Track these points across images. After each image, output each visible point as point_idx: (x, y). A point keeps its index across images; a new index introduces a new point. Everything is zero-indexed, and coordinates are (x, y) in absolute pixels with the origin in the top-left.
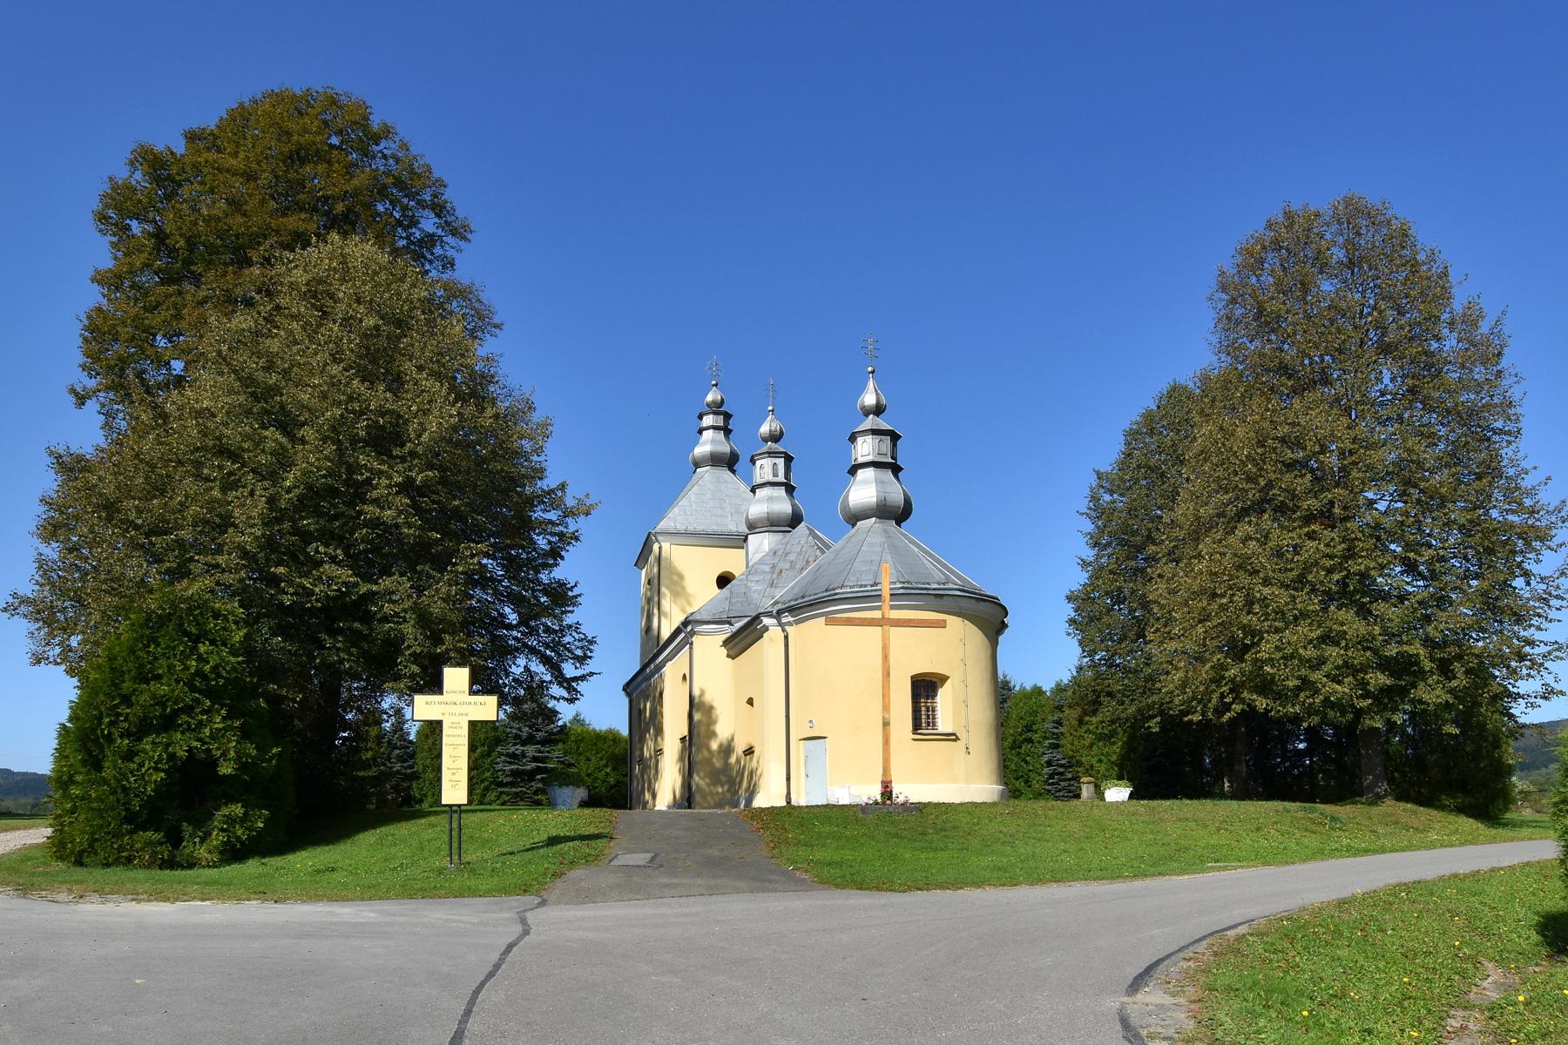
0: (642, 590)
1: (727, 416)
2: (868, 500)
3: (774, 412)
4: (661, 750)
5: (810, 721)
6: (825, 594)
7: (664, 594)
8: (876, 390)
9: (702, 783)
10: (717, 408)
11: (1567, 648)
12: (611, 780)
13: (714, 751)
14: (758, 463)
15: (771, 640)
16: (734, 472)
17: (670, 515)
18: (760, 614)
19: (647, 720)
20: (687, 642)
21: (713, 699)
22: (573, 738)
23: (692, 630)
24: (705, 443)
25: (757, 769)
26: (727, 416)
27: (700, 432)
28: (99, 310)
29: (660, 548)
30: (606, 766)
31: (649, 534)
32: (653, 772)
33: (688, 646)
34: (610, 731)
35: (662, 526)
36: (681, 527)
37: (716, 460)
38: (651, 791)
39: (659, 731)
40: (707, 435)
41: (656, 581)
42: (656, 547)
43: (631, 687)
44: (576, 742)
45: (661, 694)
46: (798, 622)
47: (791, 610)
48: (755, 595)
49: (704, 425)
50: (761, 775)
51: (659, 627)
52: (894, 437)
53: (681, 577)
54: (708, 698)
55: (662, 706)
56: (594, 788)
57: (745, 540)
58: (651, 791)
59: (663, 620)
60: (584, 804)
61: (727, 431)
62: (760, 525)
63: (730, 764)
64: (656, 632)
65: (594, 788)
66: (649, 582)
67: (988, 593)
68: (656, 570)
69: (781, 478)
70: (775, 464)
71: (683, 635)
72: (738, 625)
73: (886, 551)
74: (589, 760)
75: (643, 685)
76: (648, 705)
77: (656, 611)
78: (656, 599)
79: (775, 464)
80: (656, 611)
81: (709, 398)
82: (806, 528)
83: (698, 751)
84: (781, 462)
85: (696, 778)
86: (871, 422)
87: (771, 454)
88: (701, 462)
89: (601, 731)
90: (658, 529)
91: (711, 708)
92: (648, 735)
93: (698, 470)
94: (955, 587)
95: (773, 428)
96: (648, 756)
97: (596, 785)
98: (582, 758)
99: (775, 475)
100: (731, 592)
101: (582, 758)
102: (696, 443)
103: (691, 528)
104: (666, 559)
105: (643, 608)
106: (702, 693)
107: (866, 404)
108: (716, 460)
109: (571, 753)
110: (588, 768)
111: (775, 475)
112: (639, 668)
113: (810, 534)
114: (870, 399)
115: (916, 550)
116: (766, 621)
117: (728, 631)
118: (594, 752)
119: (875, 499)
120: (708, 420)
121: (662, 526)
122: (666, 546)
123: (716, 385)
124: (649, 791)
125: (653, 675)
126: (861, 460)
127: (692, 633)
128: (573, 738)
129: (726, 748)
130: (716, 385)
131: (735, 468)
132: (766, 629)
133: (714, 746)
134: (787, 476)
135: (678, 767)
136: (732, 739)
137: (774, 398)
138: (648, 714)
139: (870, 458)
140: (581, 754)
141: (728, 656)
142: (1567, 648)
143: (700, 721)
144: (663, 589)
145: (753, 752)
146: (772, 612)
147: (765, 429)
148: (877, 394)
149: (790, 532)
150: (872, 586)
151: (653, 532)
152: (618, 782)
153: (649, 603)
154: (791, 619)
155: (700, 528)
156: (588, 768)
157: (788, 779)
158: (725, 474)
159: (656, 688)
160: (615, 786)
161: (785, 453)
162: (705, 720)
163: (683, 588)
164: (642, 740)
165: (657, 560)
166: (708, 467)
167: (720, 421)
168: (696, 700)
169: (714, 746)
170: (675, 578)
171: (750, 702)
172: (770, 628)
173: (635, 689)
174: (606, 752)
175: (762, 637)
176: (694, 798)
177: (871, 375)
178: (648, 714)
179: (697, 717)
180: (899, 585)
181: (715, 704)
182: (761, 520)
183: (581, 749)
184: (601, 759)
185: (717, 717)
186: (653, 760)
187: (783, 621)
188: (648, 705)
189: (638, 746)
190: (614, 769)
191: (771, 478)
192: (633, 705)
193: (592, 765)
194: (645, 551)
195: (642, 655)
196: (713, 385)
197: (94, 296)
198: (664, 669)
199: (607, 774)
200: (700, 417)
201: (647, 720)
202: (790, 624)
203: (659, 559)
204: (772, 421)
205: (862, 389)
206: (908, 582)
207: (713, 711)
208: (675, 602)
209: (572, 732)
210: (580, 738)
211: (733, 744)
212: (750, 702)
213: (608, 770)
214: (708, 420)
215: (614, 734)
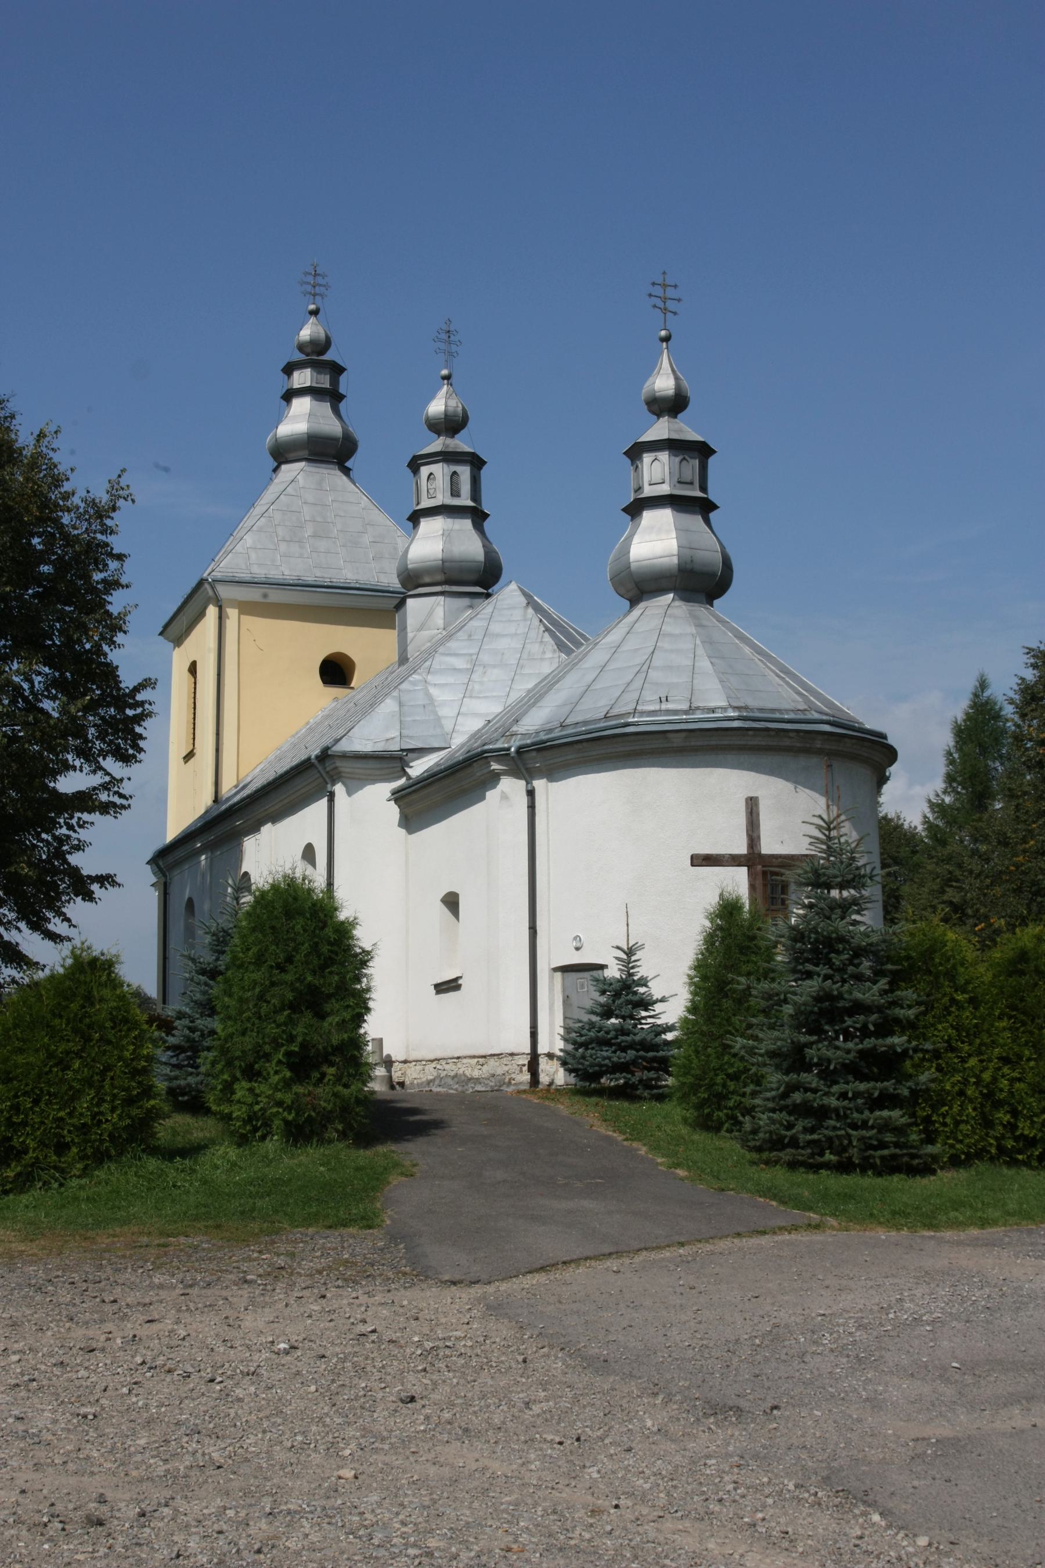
1: (336, 370)
3: (453, 380)
5: (575, 938)
6: (602, 725)
8: (673, 371)
14: (425, 471)
16: (346, 471)
24: (296, 419)
28: (126, 759)
33: (324, 801)
40: (302, 405)
43: (170, 859)
49: (296, 386)
52: (702, 451)
57: (401, 604)
62: (427, 580)
67: (868, 726)
69: (465, 500)
70: (455, 473)
73: (700, 651)
79: (455, 473)
81: (306, 334)
82: (519, 593)
84: (465, 472)
86: (661, 429)
87: (448, 457)
93: (284, 467)
94: (825, 718)
100: (401, 705)
111: (455, 493)
113: (528, 603)
114: (664, 383)
115: (747, 650)
119: (675, 560)
121: (227, 565)
123: (315, 313)
126: (648, 491)
131: (348, 464)
134: (476, 494)
139: (665, 489)
146: (509, 749)
147: (437, 407)
148: (677, 378)
150: (686, 712)
158: (333, 476)
166: (303, 464)
167: (325, 381)
171: (452, 902)
177: (664, 344)
180: (732, 714)
182: (429, 570)
197: (373, 996)
204: (447, 398)
205: (650, 368)
206: (746, 708)
212: (452, 902)
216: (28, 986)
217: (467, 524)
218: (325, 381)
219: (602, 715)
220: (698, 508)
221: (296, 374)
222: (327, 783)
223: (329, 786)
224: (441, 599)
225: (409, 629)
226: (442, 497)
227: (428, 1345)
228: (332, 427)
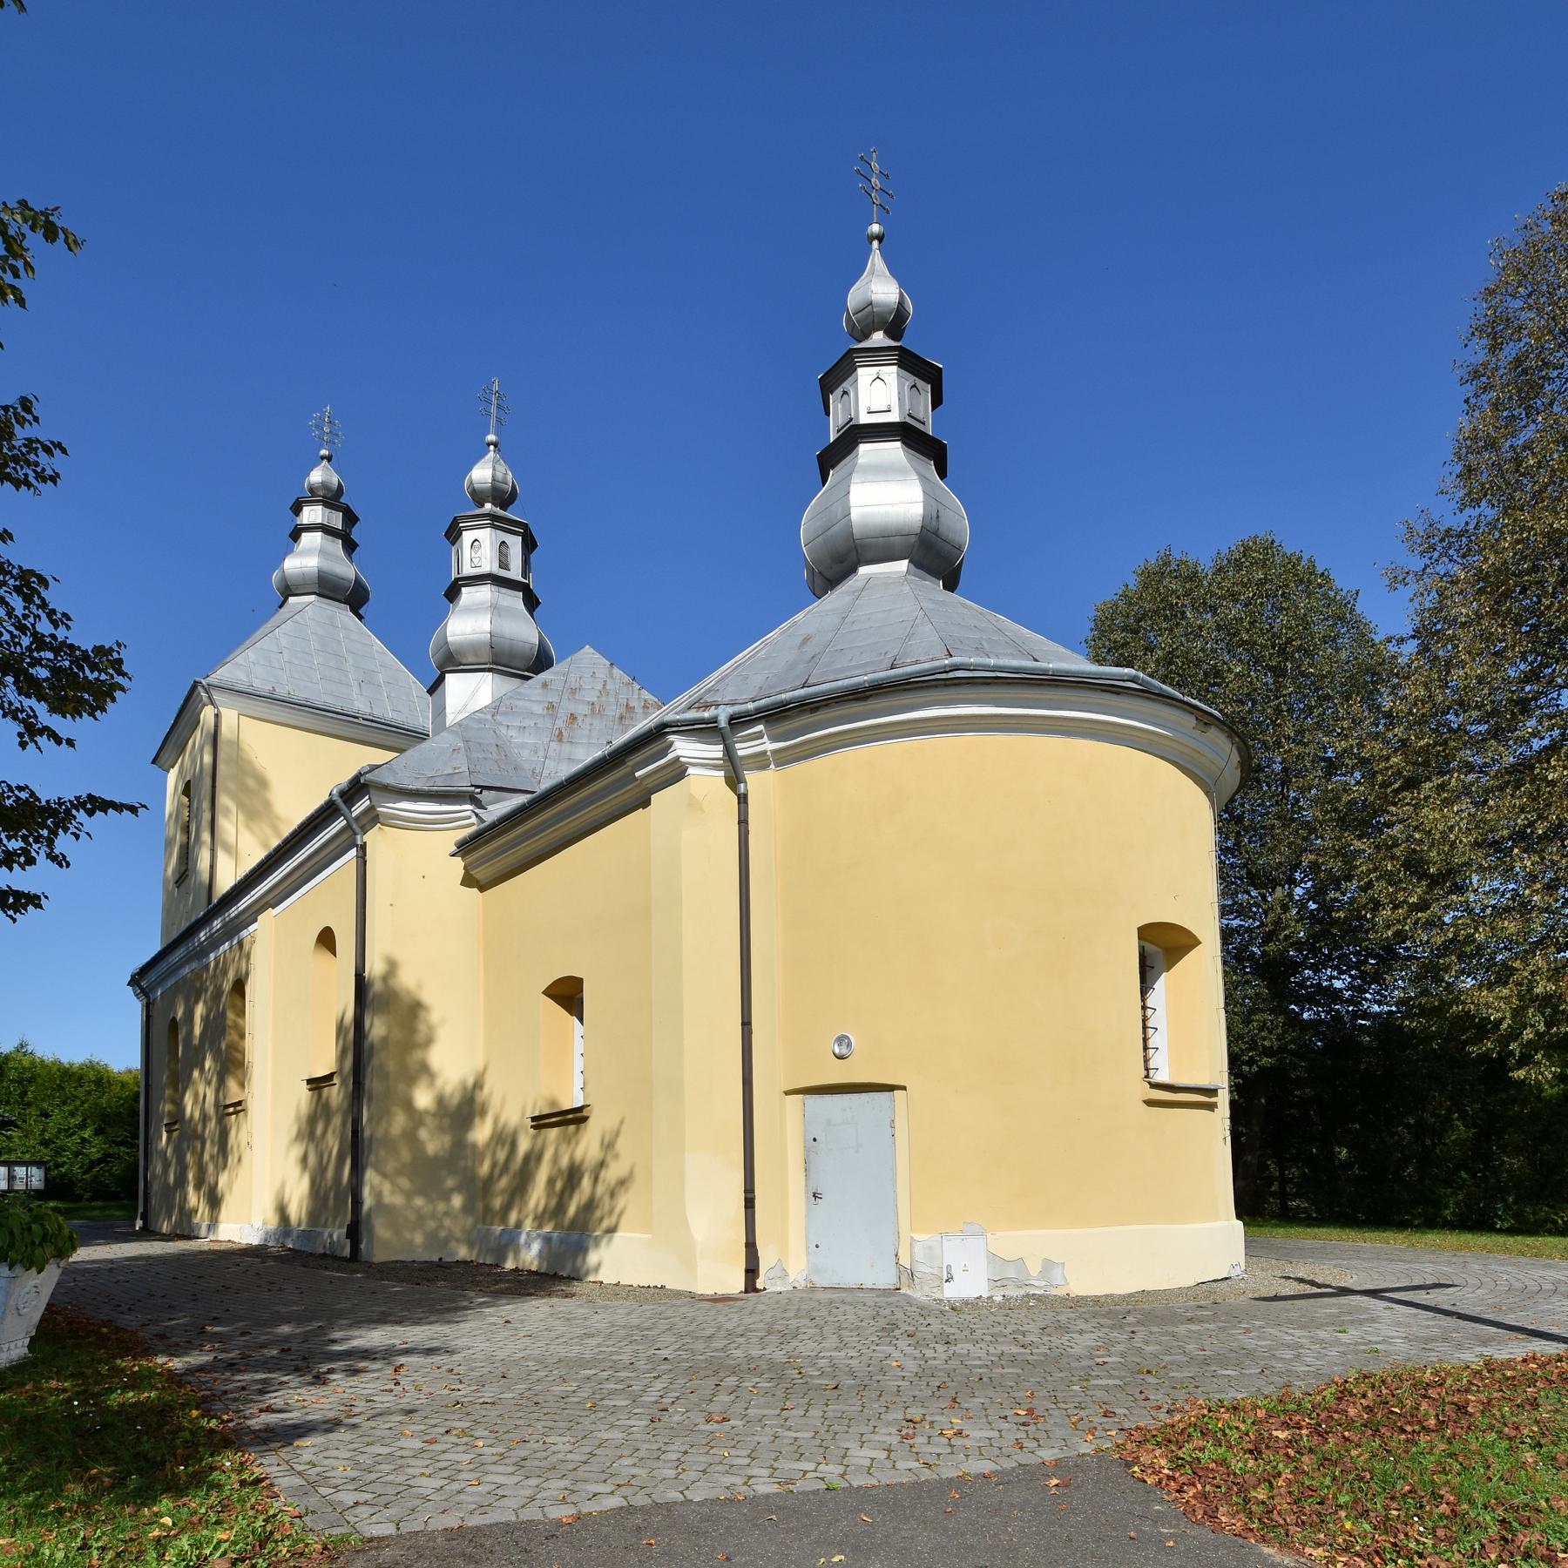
0: (169, 806)
2: (882, 509)
4: (239, 1103)
5: (841, 1040)
7: (227, 811)
9: (391, 1197)
10: (331, 498)
11: (1, 1101)
12: (94, 1152)
13: (427, 1112)
14: (468, 537)
15: (694, 804)
16: (360, 617)
17: (239, 660)
18: (665, 725)
19: (196, 1042)
20: (349, 840)
21: (420, 986)
22: (13, 1075)
23: (371, 808)
24: (307, 553)
25: (602, 1164)
26: (350, 518)
27: (296, 535)
29: (217, 716)
30: (83, 1126)
31: (196, 685)
32: (210, 1150)
33: (353, 852)
34: (91, 1066)
35: (222, 674)
36: (260, 684)
37: (326, 587)
38: (205, 1188)
39: (232, 1064)
40: (310, 540)
41: (208, 782)
42: (207, 714)
43: (153, 976)
44: (20, 1083)
45: (239, 987)
46: (784, 759)
47: (776, 715)
48: (525, 754)
50: (622, 1183)
51: (212, 867)
53: (263, 783)
54: (407, 979)
55: (241, 1012)
56: (58, 1166)
58: (205, 1188)
59: (222, 857)
60: (39, 1273)
61: (350, 546)
62: (471, 660)
63: (474, 1146)
64: (205, 876)
65: (58, 1166)
66: (187, 791)
68: (207, 759)
71: (340, 823)
72: (498, 808)
74: (47, 1116)
75: (186, 971)
76: (200, 1010)
77: (206, 836)
78: (207, 816)
80: (206, 836)
83: (384, 1115)
84: (515, 543)
85: (371, 1176)
87: (496, 522)
88: (297, 586)
89: (71, 1065)
90: (214, 679)
91: (415, 1008)
92: (196, 1074)
93: (291, 600)
95: (499, 476)
96: (197, 1115)
97: (60, 1160)
98: (33, 1111)
99: (504, 565)
101: (33, 1111)
102: (289, 551)
103: (281, 692)
104: (230, 742)
105: (169, 843)
106: (392, 967)
107: (874, 297)
108: (326, 587)
109: (8, 1103)
110: (44, 1131)
111: (504, 565)
112: (156, 948)
116: (683, 748)
117: (466, 819)
118: (57, 1101)
120: (313, 514)
122: (229, 717)
123: (329, 459)
124: (198, 1187)
125: (214, 943)
127: (371, 818)
128: (13, 1075)
129: (460, 1106)
130: (329, 459)
132: (677, 772)
133: (423, 1099)
135: (297, 1151)
136: (478, 1085)
137: (499, 420)
138: (197, 1030)
140: (29, 1104)
141: (468, 881)
142: (1, 1101)
143: (385, 1040)
144: (224, 800)
145: (585, 1119)
149: (528, 678)
151: (204, 682)
152: (106, 1155)
153: (186, 829)
154: (770, 746)
155: (300, 695)
156: (44, 1131)
157: (750, 1203)
158: (344, 614)
159: (225, 972)
160: (100, 1161)
161: (524, 526)
162: (397, 1034)
163: (267, 804)
164: (180, 1081)
165: (210, 741)
166: (313, 597)
167: (337, 521)
168: (378, 987)
169: (423, 1099)
170: (251, 783)
172: (691, 770)
173: (161, 980)
174: (83, 1102)
175: (645, 803)
176: (371, 1230)
178: (197, 1030)
179: (377, 1028)
181: (426, 997)
182: (474, 647)
183: (30, 1095)
184: (72, 1114)
185: (431, 1029)
186: (212, 1125)
187: (740, 753)
188: (200, 1010)
189: (168, 1092)
190: (98, 1132)
191: (496, 570)
192: (154, 1013)
193: (52, 1125)
194: (181, 726)
195: (165, 929)
196: (323, 458)
198: (252, 928)
199: (84, 1140)
200: (297, 509)
201: (196, 1042)
202: (760, 761)
203: (215, 737)
207: (422, 1014)
208: (248, 826)
209: (11, 1064)
210: (28, 1075)
211: (481, 1096)
213: (87, 1134)
214: (313, 514)
215: (99, 1072)
216: (25, 1192)
217: (516, 600)
218: (337, 521)
219: (800, 682)
220: (441, 1154)
221: (306, 510)
222: (355, 834)
223: (359, 837)
224: (490, 675)
225: (448, 710)
226: (488, 564)
227: (270, 1546)
228: (346, 570)
